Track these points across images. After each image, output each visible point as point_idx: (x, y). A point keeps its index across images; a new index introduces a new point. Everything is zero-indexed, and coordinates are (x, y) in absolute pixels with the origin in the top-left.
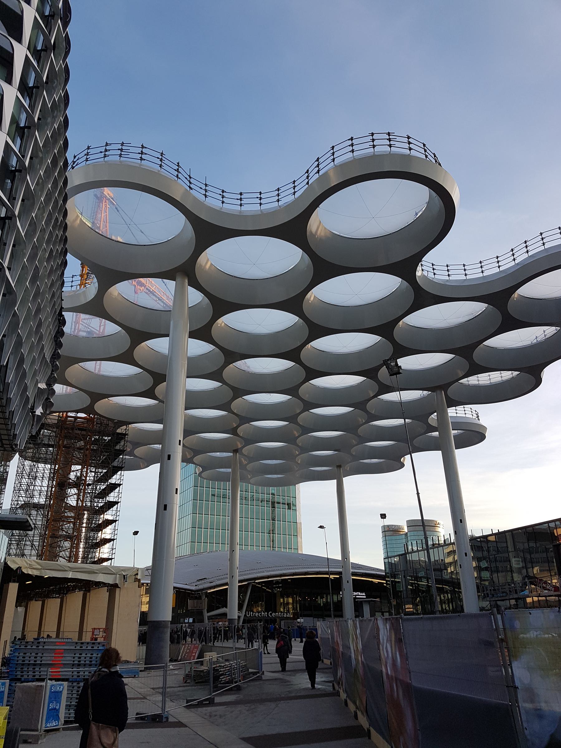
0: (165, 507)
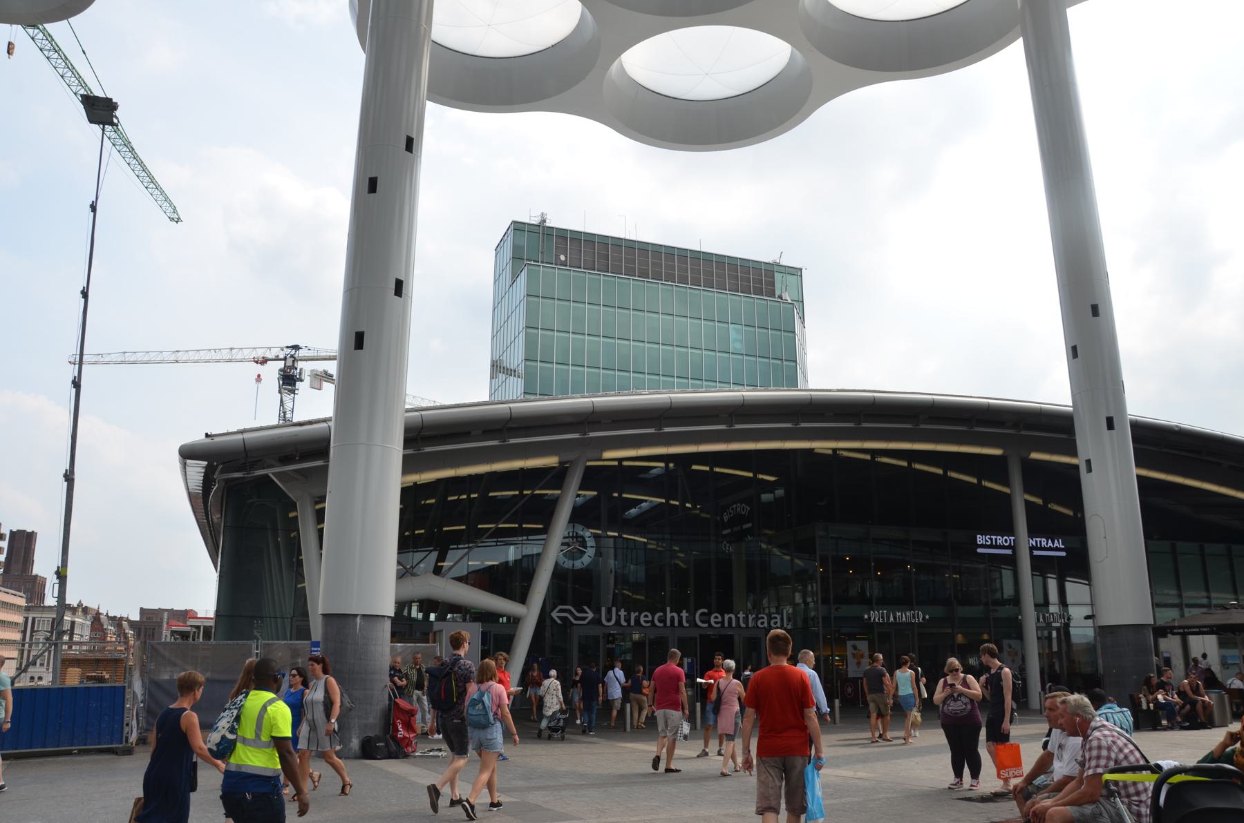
0: (1095, 310)
